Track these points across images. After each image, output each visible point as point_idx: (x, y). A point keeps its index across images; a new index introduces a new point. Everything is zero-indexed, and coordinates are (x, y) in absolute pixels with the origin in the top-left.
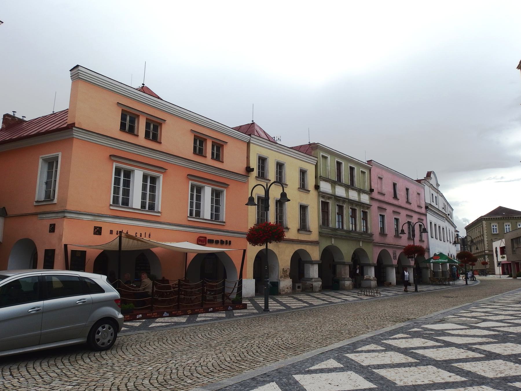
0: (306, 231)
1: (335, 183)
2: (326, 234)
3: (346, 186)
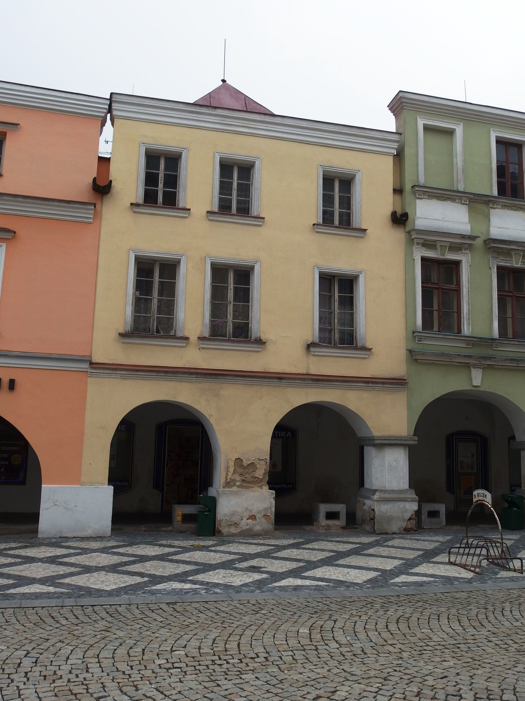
0: (356, 348)
1: (490, 201)
2: (435, 354)
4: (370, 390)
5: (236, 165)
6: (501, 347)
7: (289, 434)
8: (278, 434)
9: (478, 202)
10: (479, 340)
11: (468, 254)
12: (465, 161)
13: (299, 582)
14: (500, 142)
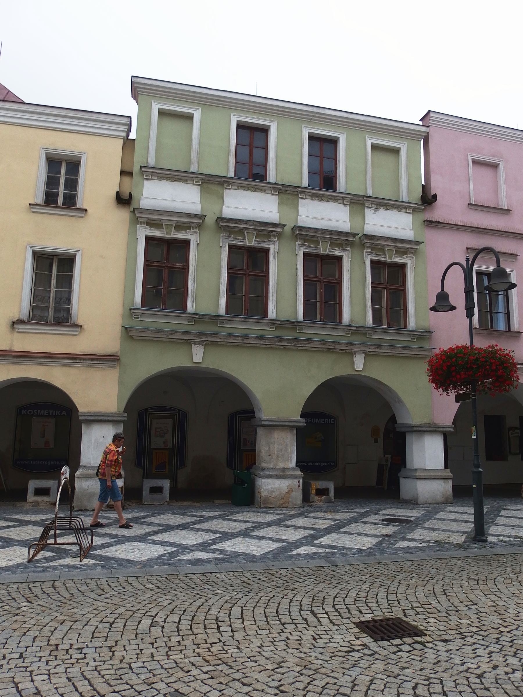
2: (149, 331)
3: (275, 189)
4: (78, 367)
5: (64, 161)
6: (227, 323)
7: (64, 413)
8: (52, 413)
9: (212, 183)
10: (201, 317)
11: (197, 233)
12: (200, 144)
13: (311, 550)
14: (312, 138)
